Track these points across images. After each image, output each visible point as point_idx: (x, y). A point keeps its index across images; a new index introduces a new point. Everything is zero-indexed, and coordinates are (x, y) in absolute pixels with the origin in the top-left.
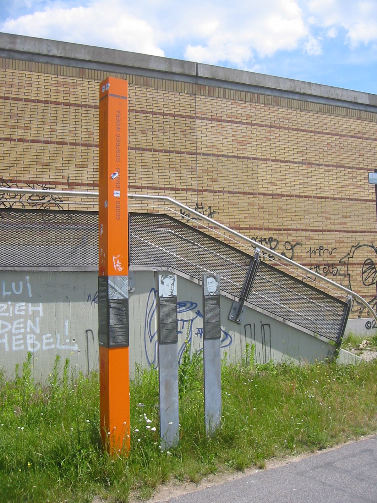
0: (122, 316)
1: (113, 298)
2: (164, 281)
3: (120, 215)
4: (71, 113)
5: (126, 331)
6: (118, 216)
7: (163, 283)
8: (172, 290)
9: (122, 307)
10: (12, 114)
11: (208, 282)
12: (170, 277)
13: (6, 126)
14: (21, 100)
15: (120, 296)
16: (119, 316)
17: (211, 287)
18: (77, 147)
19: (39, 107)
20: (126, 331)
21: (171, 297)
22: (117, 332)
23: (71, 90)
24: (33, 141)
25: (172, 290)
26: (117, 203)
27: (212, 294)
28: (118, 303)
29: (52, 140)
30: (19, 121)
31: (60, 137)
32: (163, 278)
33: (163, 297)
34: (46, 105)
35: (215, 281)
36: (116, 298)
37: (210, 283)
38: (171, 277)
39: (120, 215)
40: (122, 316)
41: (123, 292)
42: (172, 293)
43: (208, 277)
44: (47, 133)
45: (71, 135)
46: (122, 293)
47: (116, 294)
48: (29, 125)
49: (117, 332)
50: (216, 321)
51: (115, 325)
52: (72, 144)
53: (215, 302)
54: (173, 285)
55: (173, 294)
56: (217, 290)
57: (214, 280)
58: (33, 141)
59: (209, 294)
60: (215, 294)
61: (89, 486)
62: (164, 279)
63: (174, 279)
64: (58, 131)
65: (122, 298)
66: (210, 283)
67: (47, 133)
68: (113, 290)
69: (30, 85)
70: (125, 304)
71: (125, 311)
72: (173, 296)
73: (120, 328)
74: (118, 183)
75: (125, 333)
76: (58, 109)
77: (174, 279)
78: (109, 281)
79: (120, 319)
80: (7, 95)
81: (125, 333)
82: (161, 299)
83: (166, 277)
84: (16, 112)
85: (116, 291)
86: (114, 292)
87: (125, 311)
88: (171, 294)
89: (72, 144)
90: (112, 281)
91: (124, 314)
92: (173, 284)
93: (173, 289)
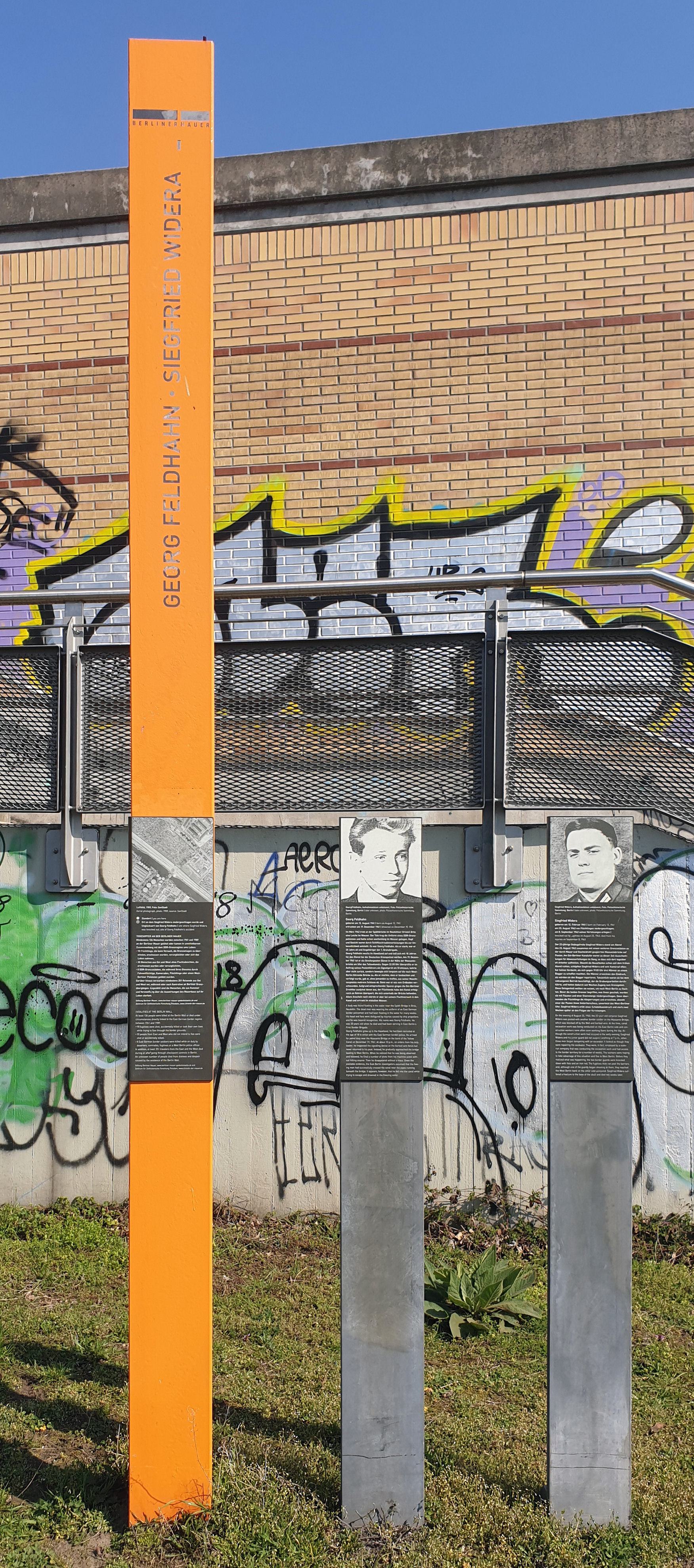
0: (183, 966)
1: (151, 900)
2: (364, 839)
3: (178, 590)
4: (436, 363)
5: (198, 1023)
6: (170, 593)
7: (358, 848)
8: (401, 878)
9: (185, 935)
10: (269, 394)
11: (570, 847)
12: (389, 824)
13: (256, 432)
14: (291, 347)
15: (176, 891)
16: (174, 965)
17: (585, 869)
18: (456, 466)
19: (343, 360)
20: (198, 1023)
21: (394, 901)
22: (163, 1023)
23: (436, 288)
24: (328, 466)
25: (401, 878)
26: (168, 541)
27: (590, 898)
28: (170, 917)
29: (382, 452)
30: (290, 411)
31: (406, 441)
32: (358, 829)
33: (361, 900)
34: (363, 349)
35: (609, 844)
36: (163, 901)
37: (583, 853)
38: (393, 825)
39: (178, 590)
40: (183, 966)
41: (192, 878)
42: (398, 886)
43: (571, 828)
44: (367, 434)
45: (437, 428)
46: (188, 881)
47: (165, 885)
48: (314, 419)
49: (163, 1023)
50: (609, 1012)
51: (155, 996)
52: (439, 458)
53: (607, 930)
54: (406, 857)
55: (405, 890)
56: (616, 881)
57: (605, 838)
58: (328, 466)
59: (578, 895)
60: (606, 899)
61: (179, 1521)
62: (364, 831)
63: (409, 834)
64: (398, 423)
65: (187, 899)
66: (583, 853)
67: (367, 434)
68: (150, 872)
69: (318, 298)
70: (201, 924)
71: (198, 947)
72: (403, 899)
73: (176, 1009)
74: (171, 465)
75: (195, 1031)
76: (398, 357)
77: (409, 834)
78: (133, 835)
79: (177, 977)
80: (255, 341)
81: (195, 1031)
82: (349, 910)
83: (373, 824)
84: (280, 385)
85: (163, 872)
86: (155, 878)
87: (198, 947)
88: (394, 891)
89: (439, 458)
90: (145, 838)
91: (194, 958)
92: (404, 854)
93: (403, 873)
